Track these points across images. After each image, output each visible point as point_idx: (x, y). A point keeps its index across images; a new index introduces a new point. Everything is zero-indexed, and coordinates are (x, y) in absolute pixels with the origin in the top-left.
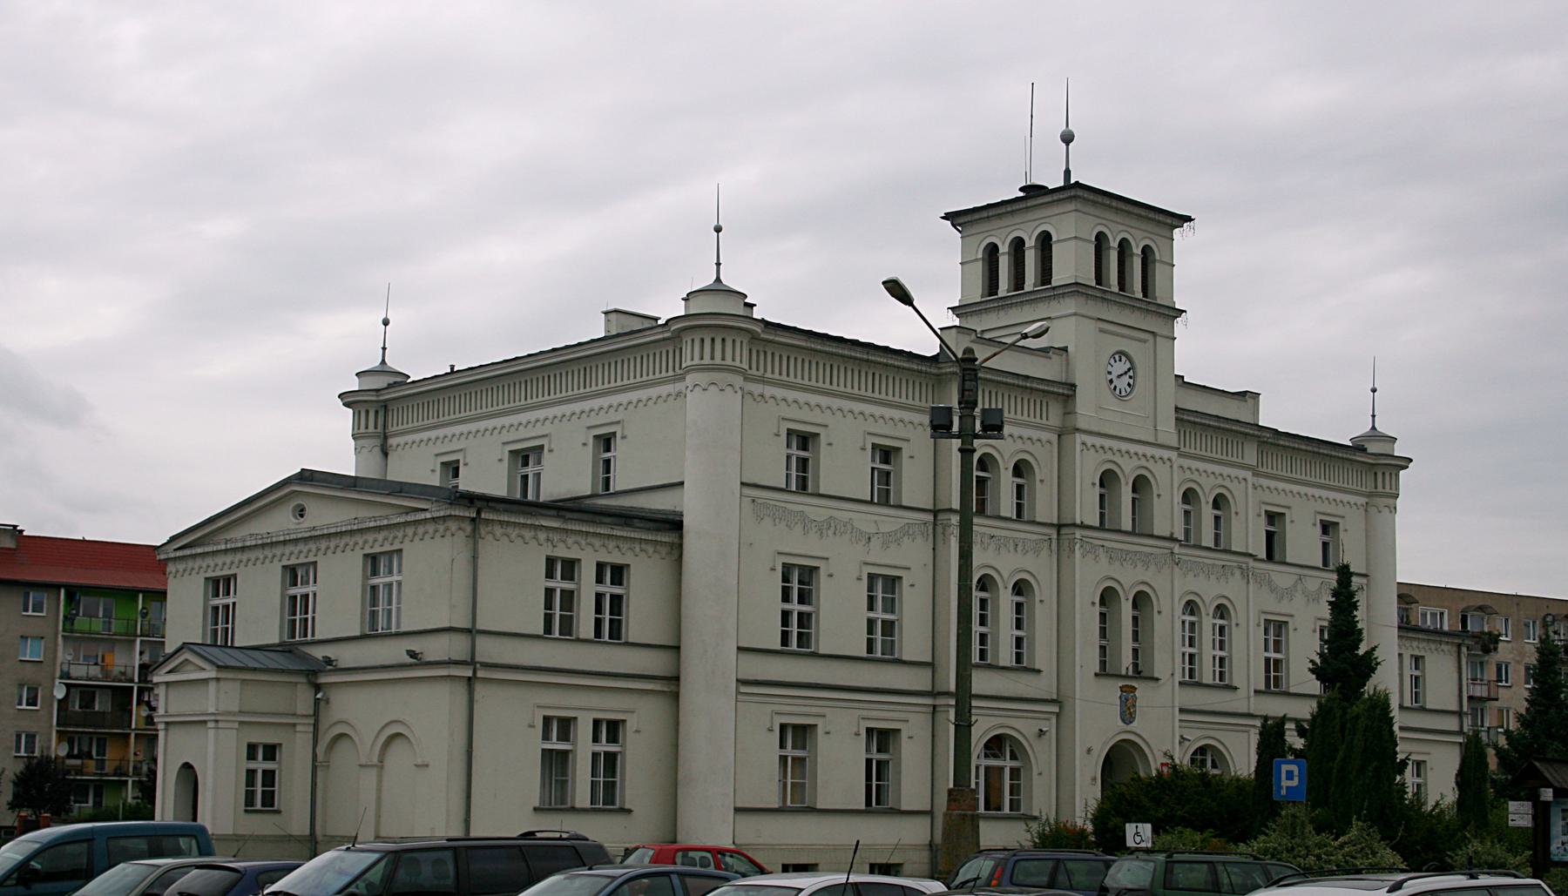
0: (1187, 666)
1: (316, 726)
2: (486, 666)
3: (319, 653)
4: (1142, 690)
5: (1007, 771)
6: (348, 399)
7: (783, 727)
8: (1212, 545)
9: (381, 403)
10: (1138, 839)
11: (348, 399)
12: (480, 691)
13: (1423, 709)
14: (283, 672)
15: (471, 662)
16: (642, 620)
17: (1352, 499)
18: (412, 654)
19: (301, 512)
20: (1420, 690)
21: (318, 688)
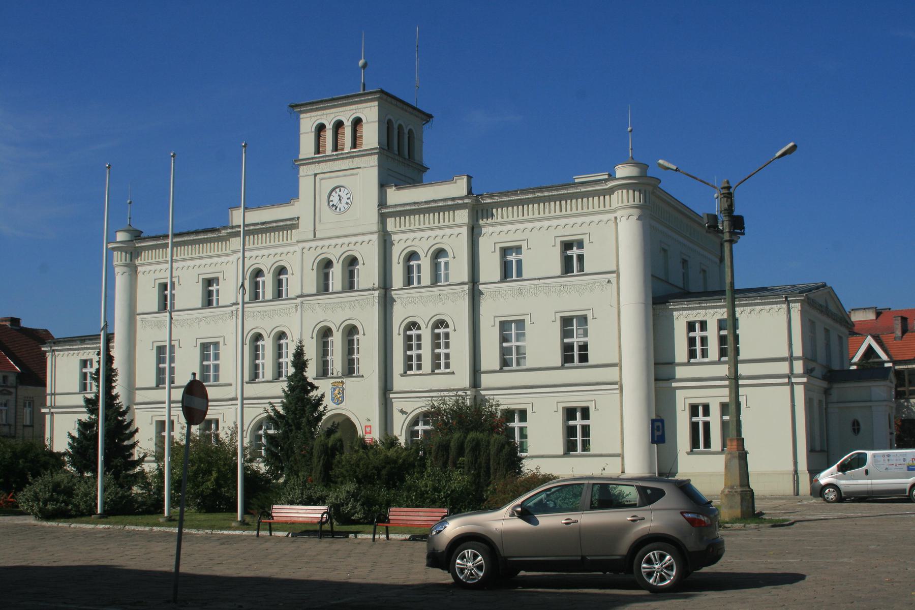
4: (349, 382)
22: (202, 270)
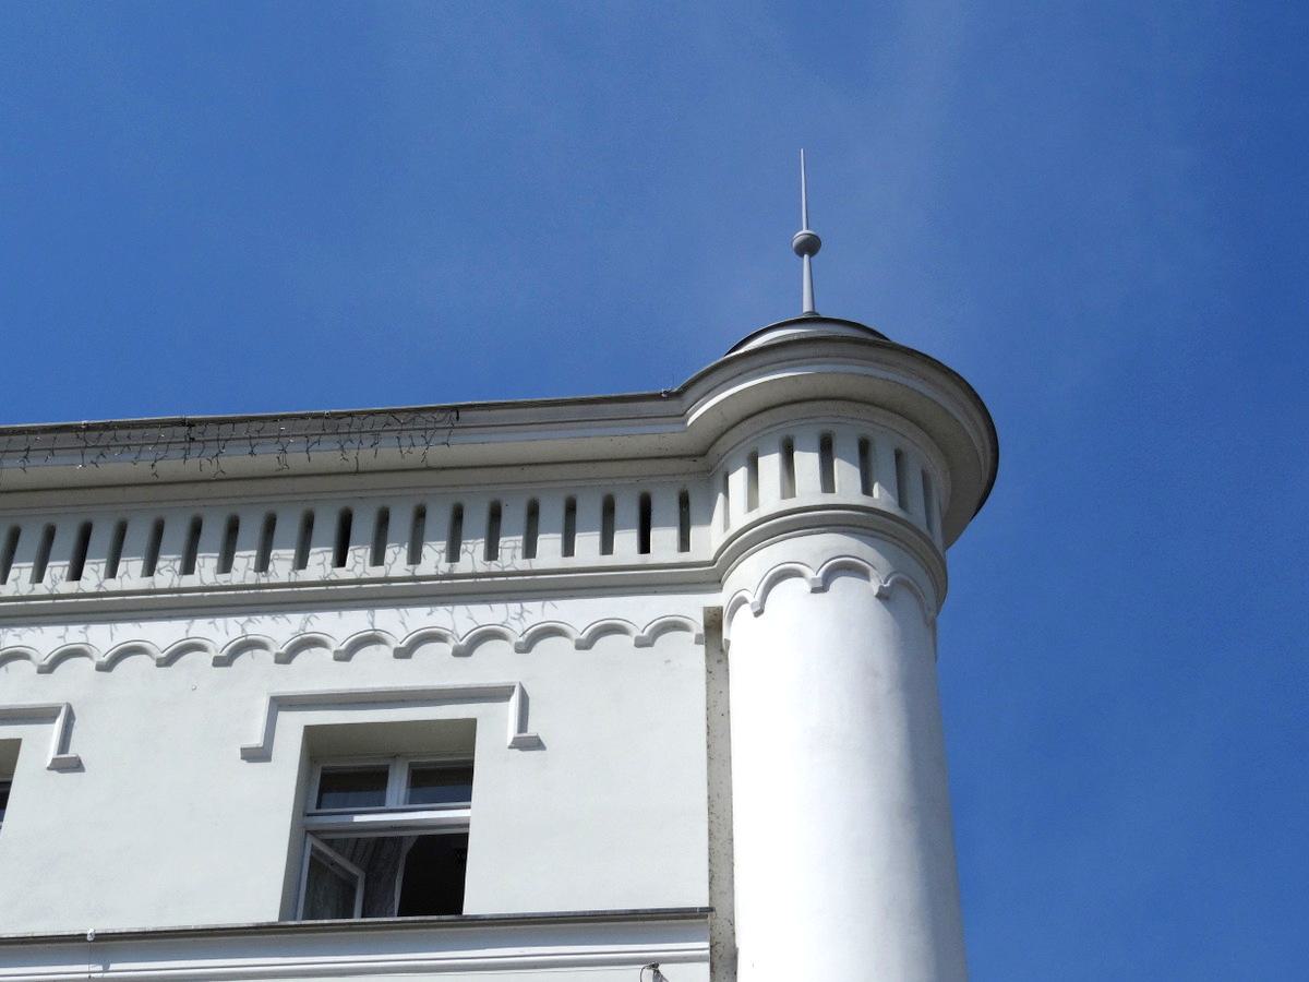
22: (316, 674)
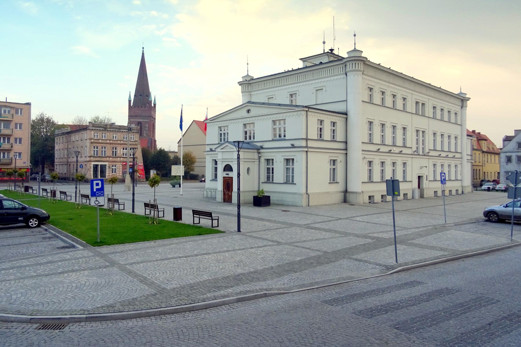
0: (319, 133)
1: (259, 161)
2: (311, 148)
3: (259, 144)
5: (107, 166)
6: (240, 84)
7: (331, 160)
8: (402, 109)
9: (248, 83)
10: (97, 203)
11: (240, 84)
12: (309, 153)
13: (323, 140)
14: (249, 149)
15: (307, 147)
16: (340, 136)
17: (339, 77)
18: (293, 145)
19: (248, 111)
20: (322, 133)
21: (259, 153)
